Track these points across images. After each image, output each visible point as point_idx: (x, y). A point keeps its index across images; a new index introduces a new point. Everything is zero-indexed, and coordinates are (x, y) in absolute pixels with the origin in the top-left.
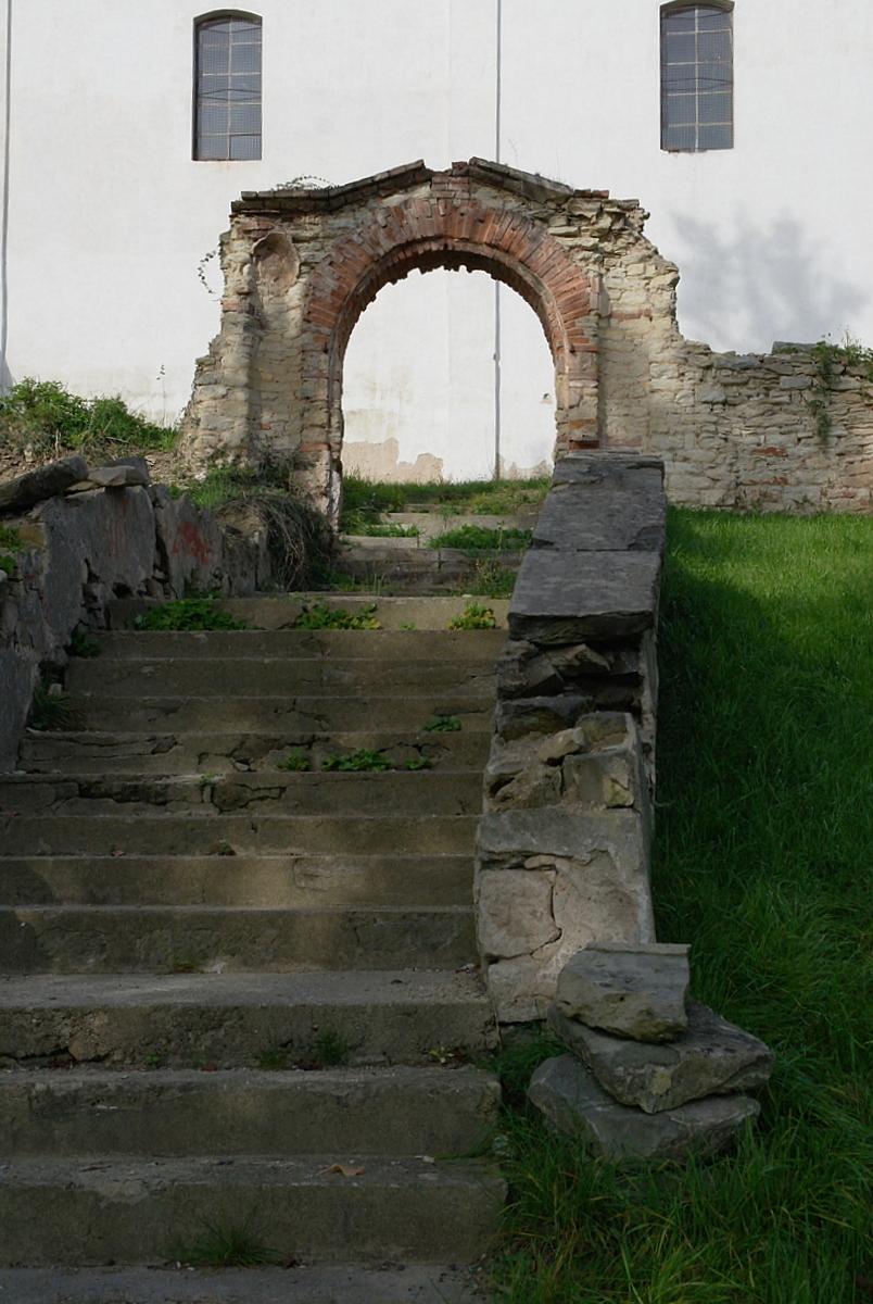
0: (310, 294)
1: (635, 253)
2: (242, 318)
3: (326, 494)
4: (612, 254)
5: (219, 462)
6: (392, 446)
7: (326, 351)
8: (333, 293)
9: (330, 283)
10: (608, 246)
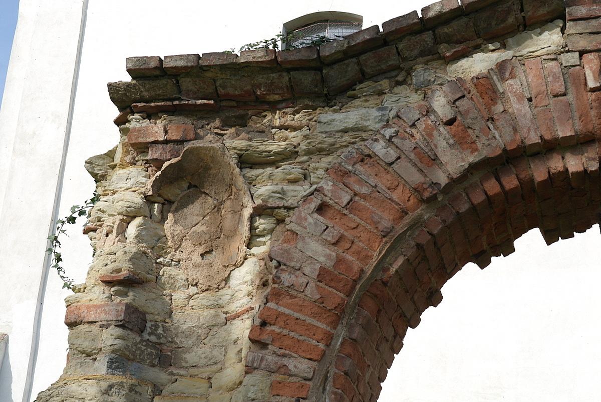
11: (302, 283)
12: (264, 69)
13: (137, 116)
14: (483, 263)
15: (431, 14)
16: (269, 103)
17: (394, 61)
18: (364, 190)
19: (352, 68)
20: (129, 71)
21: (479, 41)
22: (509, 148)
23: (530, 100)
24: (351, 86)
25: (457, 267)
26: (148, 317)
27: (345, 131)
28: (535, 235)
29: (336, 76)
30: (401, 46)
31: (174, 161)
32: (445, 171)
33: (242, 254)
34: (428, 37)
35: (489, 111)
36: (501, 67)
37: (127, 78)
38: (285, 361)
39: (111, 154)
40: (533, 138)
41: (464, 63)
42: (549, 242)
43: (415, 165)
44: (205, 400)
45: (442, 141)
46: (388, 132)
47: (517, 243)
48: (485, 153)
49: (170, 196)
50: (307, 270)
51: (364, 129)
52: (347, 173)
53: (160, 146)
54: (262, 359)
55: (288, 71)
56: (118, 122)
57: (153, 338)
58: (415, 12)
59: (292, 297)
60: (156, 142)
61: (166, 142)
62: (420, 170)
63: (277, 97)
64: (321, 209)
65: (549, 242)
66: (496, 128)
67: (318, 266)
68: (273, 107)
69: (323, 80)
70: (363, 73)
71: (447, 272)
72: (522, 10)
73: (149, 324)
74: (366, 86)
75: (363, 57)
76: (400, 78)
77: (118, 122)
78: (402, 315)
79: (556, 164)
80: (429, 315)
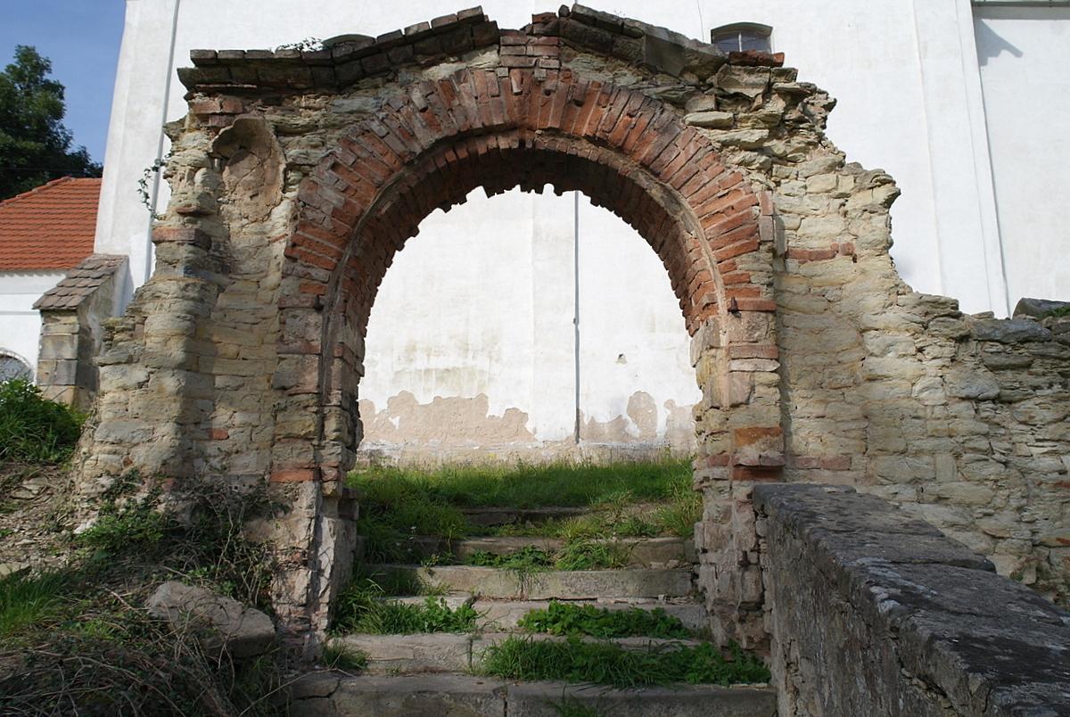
0: (299, 218)
1: (817, 159)
2: (184, 252)
3: (309, 559)
4: (783, 159)
5: (121, 501)
6: (482, 400)
7: (318, 308)
8: (336, 213)
9: (332, 197)
10: (778, 146)
12: (293, 64)
15: (411, 32)
18: (364, 155)
21: (444, 55)
23: (476, 98)
27: (351, 112)
30: (390, 54)
31: (227, 128)
33: (279, 197)
34: (409, 49)
35: (450, 104)
37: (192, 66)
38: (309, 270)
39: (182, 122)
41: (434, 69)
43: (399, 139)
45: (418, 123)
46: (381, 115)
48: (446, 133)
49: (226, 154)
50: (324, 209)
52: (353, 143)
57: (217, 254)
58: (400, 31)
62: (403, 143)
63: (303, 86)
65: (489, 196)
66: (454, 116)
67: (332, 206)
68: (300, 93)
72: (472, 35)
73: (213, 244)
74: (366, 82)
79: (492, 143)
80: (410, 242)
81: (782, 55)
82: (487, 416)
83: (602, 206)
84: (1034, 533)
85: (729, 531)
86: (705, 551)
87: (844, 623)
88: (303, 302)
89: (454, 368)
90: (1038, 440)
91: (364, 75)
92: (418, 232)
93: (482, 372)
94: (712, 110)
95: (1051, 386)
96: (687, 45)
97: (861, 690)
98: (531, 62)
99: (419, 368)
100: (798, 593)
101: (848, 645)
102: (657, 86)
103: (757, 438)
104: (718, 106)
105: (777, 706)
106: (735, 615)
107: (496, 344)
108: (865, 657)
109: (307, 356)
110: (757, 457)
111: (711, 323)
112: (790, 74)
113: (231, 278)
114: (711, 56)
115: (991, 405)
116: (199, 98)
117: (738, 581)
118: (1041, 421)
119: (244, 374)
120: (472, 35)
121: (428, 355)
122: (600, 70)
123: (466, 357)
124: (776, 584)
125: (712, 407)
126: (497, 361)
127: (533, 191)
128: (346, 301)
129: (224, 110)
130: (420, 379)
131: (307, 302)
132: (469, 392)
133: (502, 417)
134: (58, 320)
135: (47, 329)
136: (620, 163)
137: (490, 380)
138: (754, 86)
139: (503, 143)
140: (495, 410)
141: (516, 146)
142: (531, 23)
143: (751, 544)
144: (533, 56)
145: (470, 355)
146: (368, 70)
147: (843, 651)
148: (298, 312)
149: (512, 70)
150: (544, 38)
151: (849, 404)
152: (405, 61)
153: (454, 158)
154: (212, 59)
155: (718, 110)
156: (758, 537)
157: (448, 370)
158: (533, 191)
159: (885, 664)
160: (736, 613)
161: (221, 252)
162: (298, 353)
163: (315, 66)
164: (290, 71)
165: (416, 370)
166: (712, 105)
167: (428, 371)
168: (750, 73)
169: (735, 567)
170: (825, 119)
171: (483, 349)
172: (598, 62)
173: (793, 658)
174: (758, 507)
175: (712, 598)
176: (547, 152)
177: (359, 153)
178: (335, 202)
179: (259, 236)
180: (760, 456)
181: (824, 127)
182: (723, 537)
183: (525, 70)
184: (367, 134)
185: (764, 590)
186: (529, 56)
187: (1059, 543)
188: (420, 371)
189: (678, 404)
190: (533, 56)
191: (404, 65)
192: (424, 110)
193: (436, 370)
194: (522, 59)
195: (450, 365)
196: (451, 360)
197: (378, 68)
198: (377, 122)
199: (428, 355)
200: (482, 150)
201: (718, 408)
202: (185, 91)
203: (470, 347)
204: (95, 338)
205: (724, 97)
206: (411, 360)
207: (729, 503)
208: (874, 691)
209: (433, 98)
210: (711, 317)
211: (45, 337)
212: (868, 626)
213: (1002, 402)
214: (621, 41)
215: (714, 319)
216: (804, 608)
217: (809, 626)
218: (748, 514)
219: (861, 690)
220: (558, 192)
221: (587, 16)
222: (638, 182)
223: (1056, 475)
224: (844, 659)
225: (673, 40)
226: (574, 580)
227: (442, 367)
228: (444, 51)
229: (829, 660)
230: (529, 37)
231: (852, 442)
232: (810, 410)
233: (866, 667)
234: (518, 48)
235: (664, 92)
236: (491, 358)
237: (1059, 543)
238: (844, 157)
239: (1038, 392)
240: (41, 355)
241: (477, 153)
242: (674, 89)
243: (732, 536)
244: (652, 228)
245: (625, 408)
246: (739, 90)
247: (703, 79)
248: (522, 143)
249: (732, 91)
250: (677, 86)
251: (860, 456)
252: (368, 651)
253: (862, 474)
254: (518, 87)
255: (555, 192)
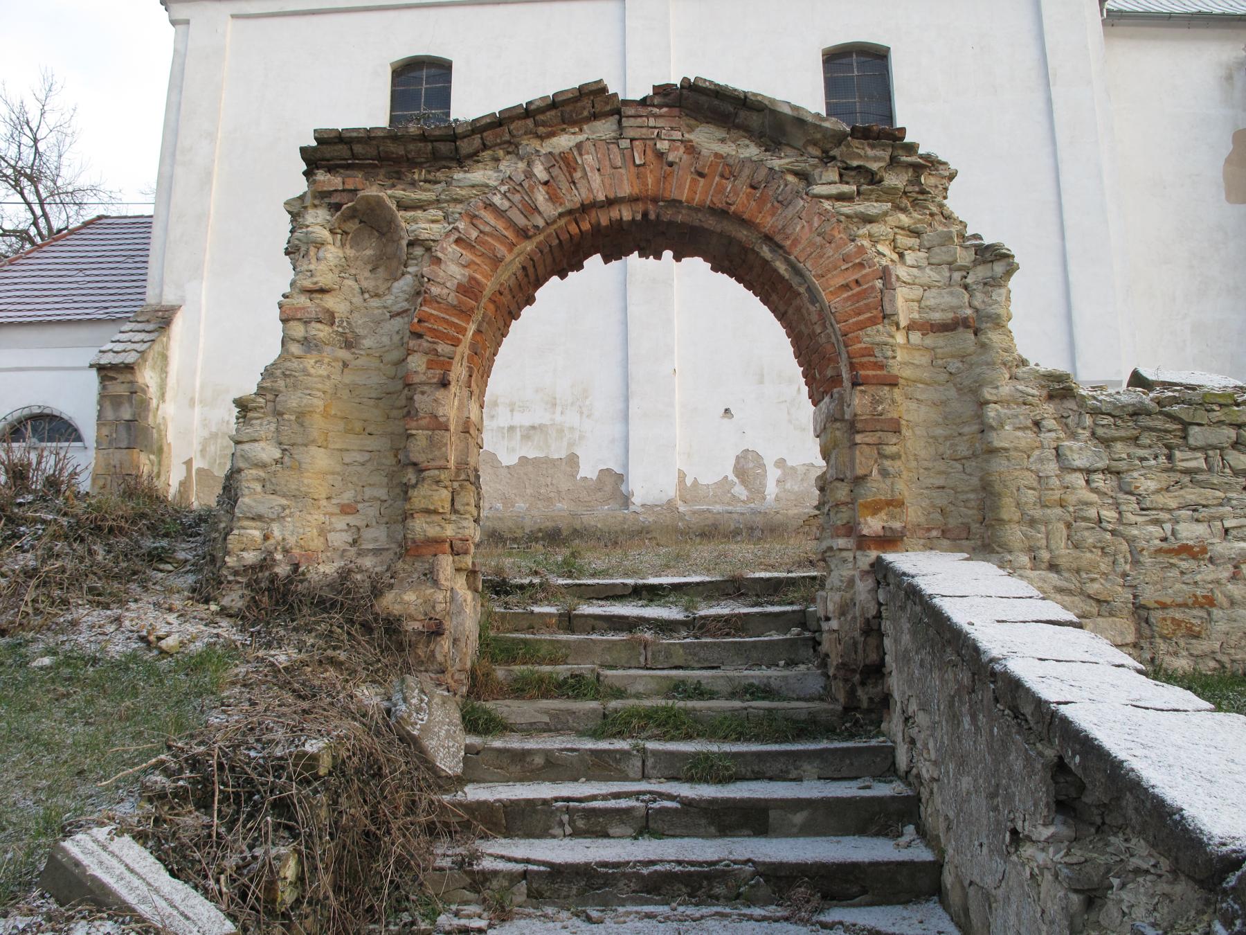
6: (573, 460)
11: (93, 189)
12: (414, 140)
13: (321, 171)
14: (563, 276)
15: (533, 107)
16: (417, 163)
17: (507, 137)
18: (487, 229)
19: (477, 141)
20: (316, 139)
21: (565, 126)
22: (585, 203)
23: (599, 170)
24: (476, 153)
25: (546, 280)
26: (336, 315)
27: (473, 186)
28: (597, 259)
29: (465, 147)
30: (512, 128)
31: (350, 204)
32: (543, 217)
33: (400, 272)
34: (530, 122)
35: (572, 177)
36: (579, 146)
37: (314, 144)
38: (435, 346)
39: (302, 198)
40: (601, 197)
41: (555, 140)
42: (606, 263)
43: (522, 213)
44: (1242, 566)
45: (540, 196)
46: (503, 188)
47: (585, 263)
48: (569, 206)
49: (346, 229)
50: (448, 284)
51: (487, 186)
52: (475, 216)
53: (339, 194)
54: (420, 345)
55: (432, 141)
56: (305, 173)
57: (340, 330)
58: (521, 105)
59: (438, 303)
60: (336, 191)
61: (344, 191)
62: (525, 216)
63: (423, 160)
64: (458, 241)
65: (606, 263)
66: (577, 189)
67: (456, 281)
68: (420, 165)
69: (457, 149)
70: (484, 145)
71: (539, 283)
72: (593, 107)
73: (337, 320)
74: (486, 154)
75: (485, 134)
76: (510, 150)
77: (305, 173)
78: (510, 313)
79: (614, 214)
80: (527, 311)
81: (903, 130)
82: (578, 478)
83: (723, 272)
84: (1135, 597)
85: (852, 600)
86: (828, 619)
87: (955, 675)
88: (430, 378)
89: (540, 425)
90: (1143, 509)
91: (485, 147)
92: (535, 300)
93: (572, 429)
94: (835, 183)
95: (1156, 457)
96: (810, 119)
97: (967, 727)
98: (653, 133)
99: (502, 425)
100: (917, 653)
101: (958, 691)
102: (781, 158)
103: (880, 510)
104: (842, 180)
105: (894, 757)
106: (857, 678)
107: (586, 397)
108: (970, 699)
109: (436, 432)
110: (880, 528)
111: (836, 396)
112: (911, 148)
113: (353, 353)
114: (834, 130)
115: (1101, 476)
116: (321, 176)
117: (860, 647)
118: (1146, 490)
119: (370, 449)
120: (593, 107)
121: (512, 411)
122: (723, 141)
123: (554, 413)
124: (896, 647)
125: (837, 479)
126: (588, 416)
127: (651, 257)
128: (471, 376)
129: (347, 187)
130: (503, 437)
131: (434, 377)
132: (558, 451)
133: (594, 478)
134: (115, 379)
135: (104, 388)
136: (742, 234)
137: (581, 438)
138: (876, 159)
139: (627, 215)
140: (588, 470)
141: (639, 217)
142: (651, 94)
143: (873, 612)
144: (655, 128)
145: (559, 409)
146: (488, 143)
147: (953, 697)
148: (426, 388)
149: (634, 142)
150: (665, 110)
151: (969, 475)
152: (526, 133)
153: (577, 231)
154: (336, 137)
155: (841, 182)
156: (880, 604)
157: (533, 428)
158: (651, 257)
159: (985, 702)
160: (858, 676)
161: (344, 328)
162: (428, 429)
163: (436, 141)
164: (411, 147)
165: (499, 427)
166: (837, 178)
167: (511, 429)
168: (872, 147)
169: (857, 634)
170: (946, 189)
171: (572, 404)
172: (720, 133)
173: (910, 712)
174: (880, 577)
175: (835, 663)
176: (671, 223)
177: (482, 227)
178: (458, 277)
179: (380, 311)
180: (883, 527)
181: (945, 198)
182: (847, 605)
183: (648, 142)
184: (489, 208)
185: (885, 654)
186: (652, 128)
187: (1156, 605)
188: (503, 428)
189: (789, 463)
190: (655, 128)
191: (525, 137)
192: (546, 183)
193: (521, 427)
194: (644, 130)
195: (537, 421)
196: (539, 416)
197: (498, 141)
198: (499, 196)
199: (512, 411)
200: (604, 221)
201: (843, 480)
202: (304, 167)
203: (558, 401)
204: (153, 396)
205: (846, 169)
206: (493, 417)
207: (853, 573)
208: (976, 726)
209: (555, 171)
210: (835, 390)
211: (103, 397)
212: (974, 674)
213: (1111, 473)
214: (743, 114)
215: (838, 393)
216: (922, 666)
217: (926, 680)
218: (870, 583)
219: (967, 727)
220: (678, 258)
221: (710, 89)
222: (762, 254)
223: (1157, 542)
224: (954, 705)
225: (795, 114)
226: (698, 649)
227: (527, 423)
228: (564, 123)
229: (942, 707)
230: (650, 109)
231: (970, 512)
232: (931, 481)
233: (971, 707)
234: (639, 120)
235: (788, 164)
236: (582, 413)
237: (1156, 605)
238: (966, 227)
239: (1145, 463)
240: (99, 417)
241: (599, 224)
242: (797, 161)
243: (855, 604)
244: (774, 297)
245: (731, 468)
246: (861, 163)
247: (825, 152)
248: (645, 215)
249: (855, 163)
250: (799, 159)
251: (978, 525)
252: (504, 715)
253: (979, 543)
254: (640, 158)
255: (674, 258)
